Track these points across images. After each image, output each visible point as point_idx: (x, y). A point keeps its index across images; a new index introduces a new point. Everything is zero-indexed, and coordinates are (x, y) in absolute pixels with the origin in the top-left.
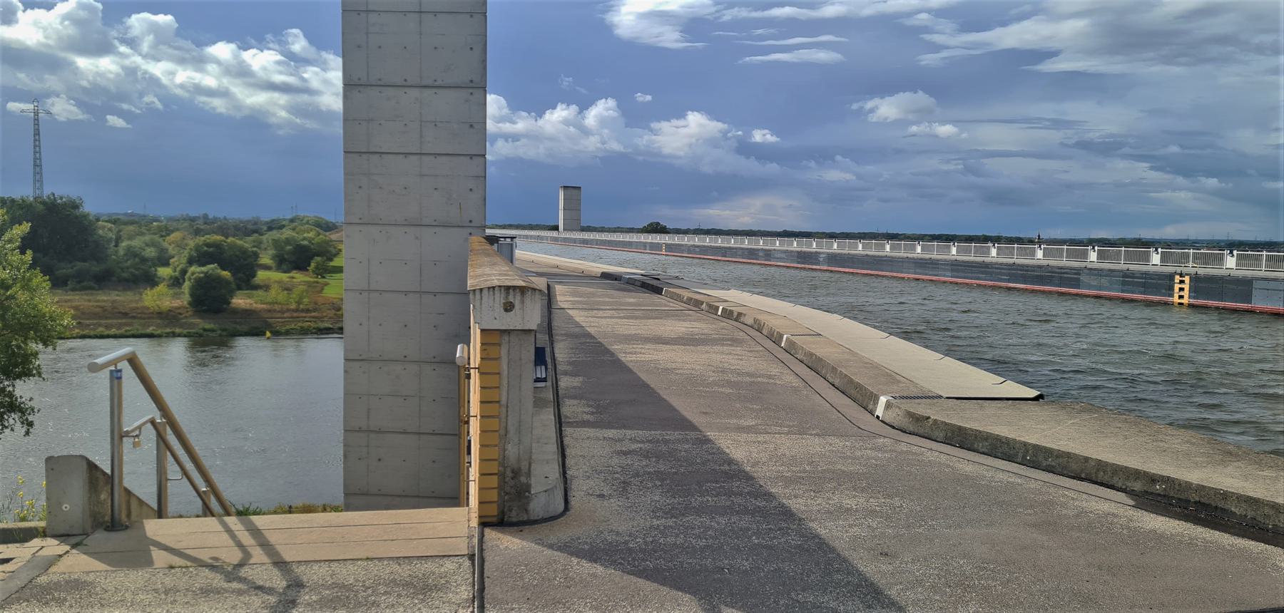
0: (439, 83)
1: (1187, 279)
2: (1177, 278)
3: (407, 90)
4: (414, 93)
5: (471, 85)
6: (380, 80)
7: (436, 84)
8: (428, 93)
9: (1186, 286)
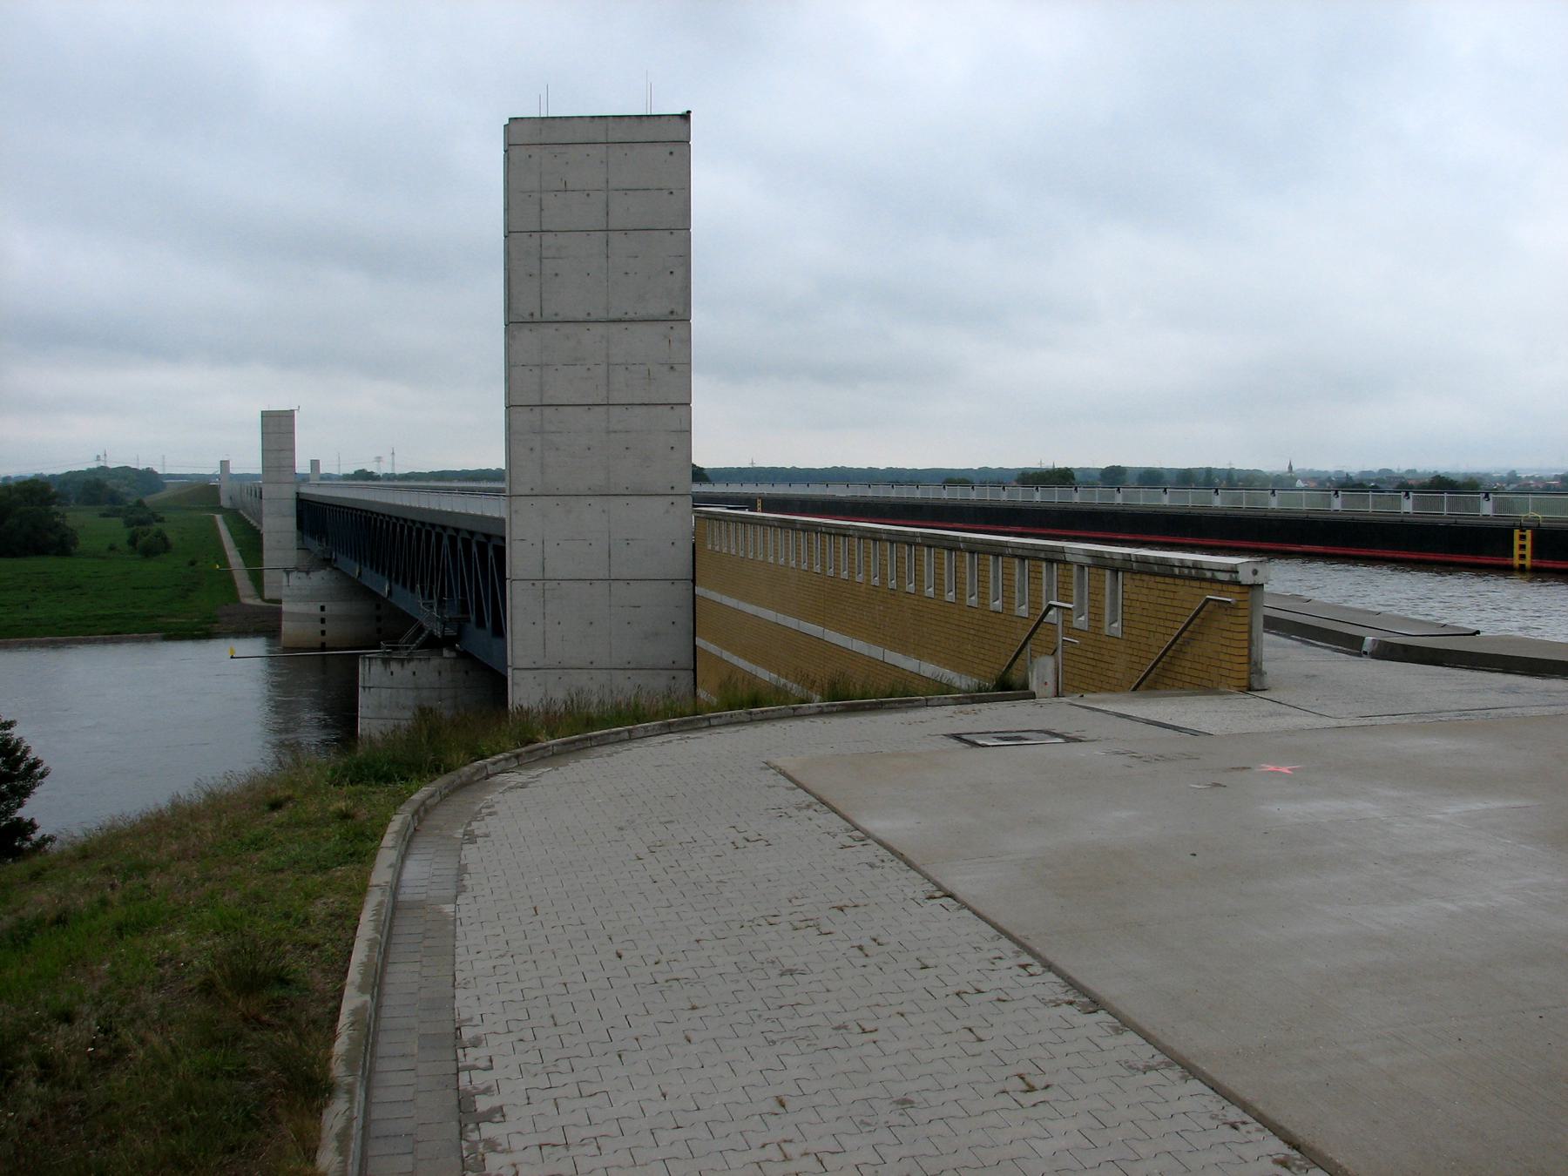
0: (631, 315)
1: (1528, 533)
2: (1517, 533)
3: (590, 326)
4: (599, 329)
5: (672, 317)
6: (556, 315)
7: (627, 317)
8: (614, 327)
9: (1528, 543)
